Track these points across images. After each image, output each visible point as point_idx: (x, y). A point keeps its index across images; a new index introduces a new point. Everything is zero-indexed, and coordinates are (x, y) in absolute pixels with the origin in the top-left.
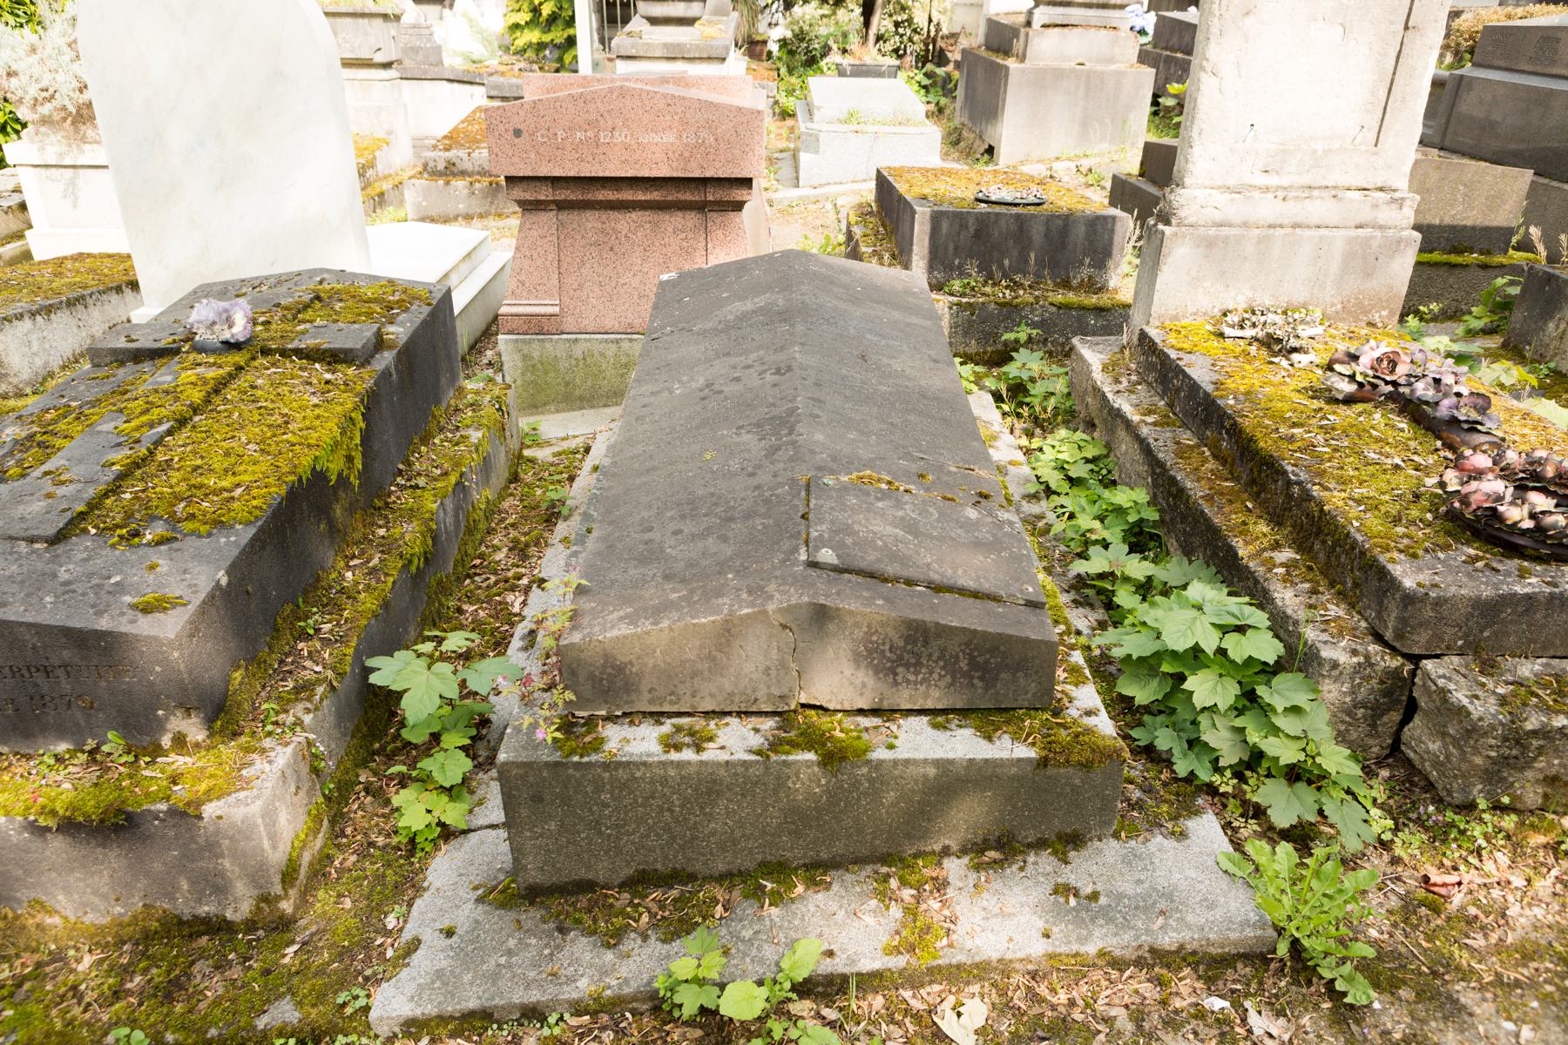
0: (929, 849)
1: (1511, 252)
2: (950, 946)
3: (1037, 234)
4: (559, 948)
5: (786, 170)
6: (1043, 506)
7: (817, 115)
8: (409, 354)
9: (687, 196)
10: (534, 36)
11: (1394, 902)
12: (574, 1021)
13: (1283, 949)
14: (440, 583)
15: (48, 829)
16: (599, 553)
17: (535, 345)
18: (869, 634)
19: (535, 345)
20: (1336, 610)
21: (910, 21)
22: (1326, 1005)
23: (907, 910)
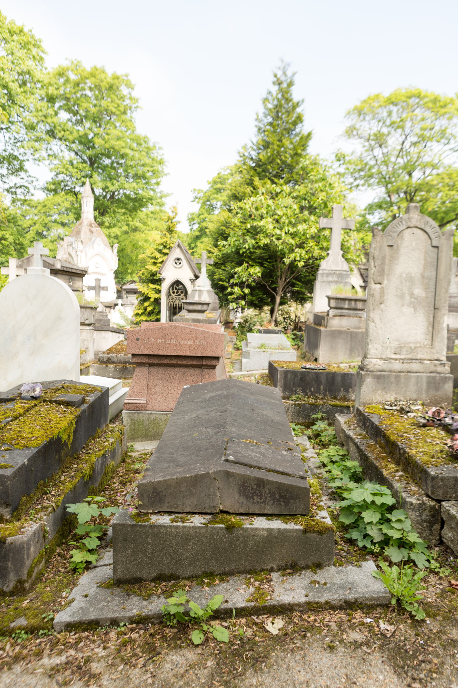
0: (265, 568)
2: (271, 599)
3: (323, 379)
4: (127, 600)
5: (237, 366)
6: (323, 470)
7: (249, 345)
8: (92, 406)
9: (195, 363)
10: (144, 318)
11: (438, 591)
12: (129, 626)
13: (394, 602)
14: (93, 489)
16: (154, 461)
18: (244, 483)
20: (413, 488)
21: (289, 317)
22: (409, 621)
23: (256, 588)
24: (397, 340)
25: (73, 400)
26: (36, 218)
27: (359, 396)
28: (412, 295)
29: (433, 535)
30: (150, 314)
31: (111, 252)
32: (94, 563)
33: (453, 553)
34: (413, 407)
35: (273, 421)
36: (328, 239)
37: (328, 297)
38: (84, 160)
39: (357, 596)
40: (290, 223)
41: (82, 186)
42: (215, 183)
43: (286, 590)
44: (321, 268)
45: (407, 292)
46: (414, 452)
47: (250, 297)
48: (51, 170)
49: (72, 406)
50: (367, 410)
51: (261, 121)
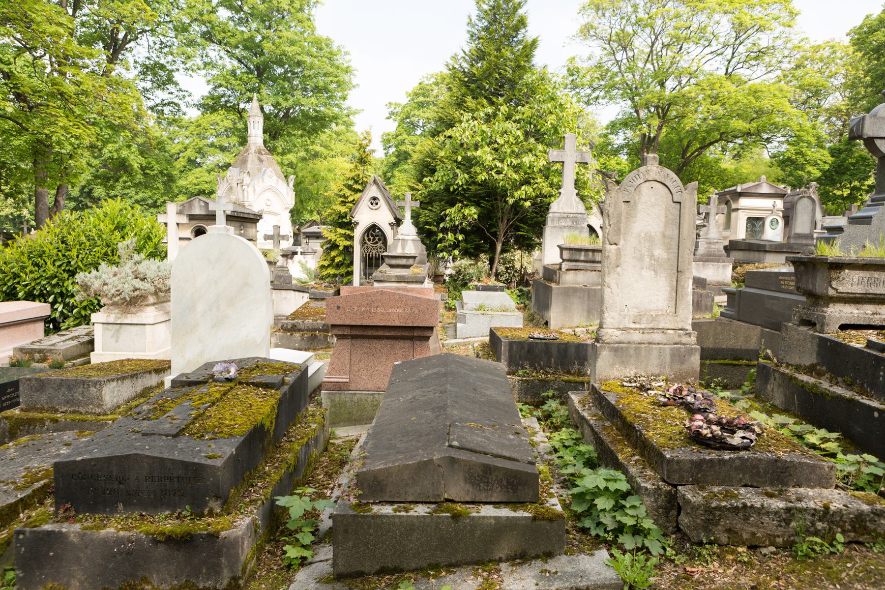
1: (760, 360)
3: (554, 351)
5: (450, 332)
6: (555, 456)
8: (293, 387)
9: (406, 334)
10: (331, 271)
15: (160, 542)
17: (337, 396)
18: (470, 469)
19: (337, 396)
20: (649, 473)
21: (513, 267)
24: (636, 308)
25: (273, 381)
26: (187, 141)
27: (595, 371)
28: (652, 256)
29: (669, 522)
30: (338, 266)
31: (285, 185)
32: (310, 559)
33: (689, 540)
34: (653, 384)
35: (498, 402)
36: (560, 173)
37: (559, 246)
38: (249, 68)
39: (589, 583)
40: (513, 152)
41: (248, 102)
42: (417, 95)
43: (515, 579)
44: (551, 211)
45: (647, 253)
46: (650, 434)
47: (463, 245)
48: (209, 82)
49: (272, 388)
50: (603, 387)
51: (473, 26)
